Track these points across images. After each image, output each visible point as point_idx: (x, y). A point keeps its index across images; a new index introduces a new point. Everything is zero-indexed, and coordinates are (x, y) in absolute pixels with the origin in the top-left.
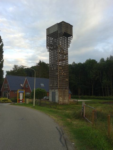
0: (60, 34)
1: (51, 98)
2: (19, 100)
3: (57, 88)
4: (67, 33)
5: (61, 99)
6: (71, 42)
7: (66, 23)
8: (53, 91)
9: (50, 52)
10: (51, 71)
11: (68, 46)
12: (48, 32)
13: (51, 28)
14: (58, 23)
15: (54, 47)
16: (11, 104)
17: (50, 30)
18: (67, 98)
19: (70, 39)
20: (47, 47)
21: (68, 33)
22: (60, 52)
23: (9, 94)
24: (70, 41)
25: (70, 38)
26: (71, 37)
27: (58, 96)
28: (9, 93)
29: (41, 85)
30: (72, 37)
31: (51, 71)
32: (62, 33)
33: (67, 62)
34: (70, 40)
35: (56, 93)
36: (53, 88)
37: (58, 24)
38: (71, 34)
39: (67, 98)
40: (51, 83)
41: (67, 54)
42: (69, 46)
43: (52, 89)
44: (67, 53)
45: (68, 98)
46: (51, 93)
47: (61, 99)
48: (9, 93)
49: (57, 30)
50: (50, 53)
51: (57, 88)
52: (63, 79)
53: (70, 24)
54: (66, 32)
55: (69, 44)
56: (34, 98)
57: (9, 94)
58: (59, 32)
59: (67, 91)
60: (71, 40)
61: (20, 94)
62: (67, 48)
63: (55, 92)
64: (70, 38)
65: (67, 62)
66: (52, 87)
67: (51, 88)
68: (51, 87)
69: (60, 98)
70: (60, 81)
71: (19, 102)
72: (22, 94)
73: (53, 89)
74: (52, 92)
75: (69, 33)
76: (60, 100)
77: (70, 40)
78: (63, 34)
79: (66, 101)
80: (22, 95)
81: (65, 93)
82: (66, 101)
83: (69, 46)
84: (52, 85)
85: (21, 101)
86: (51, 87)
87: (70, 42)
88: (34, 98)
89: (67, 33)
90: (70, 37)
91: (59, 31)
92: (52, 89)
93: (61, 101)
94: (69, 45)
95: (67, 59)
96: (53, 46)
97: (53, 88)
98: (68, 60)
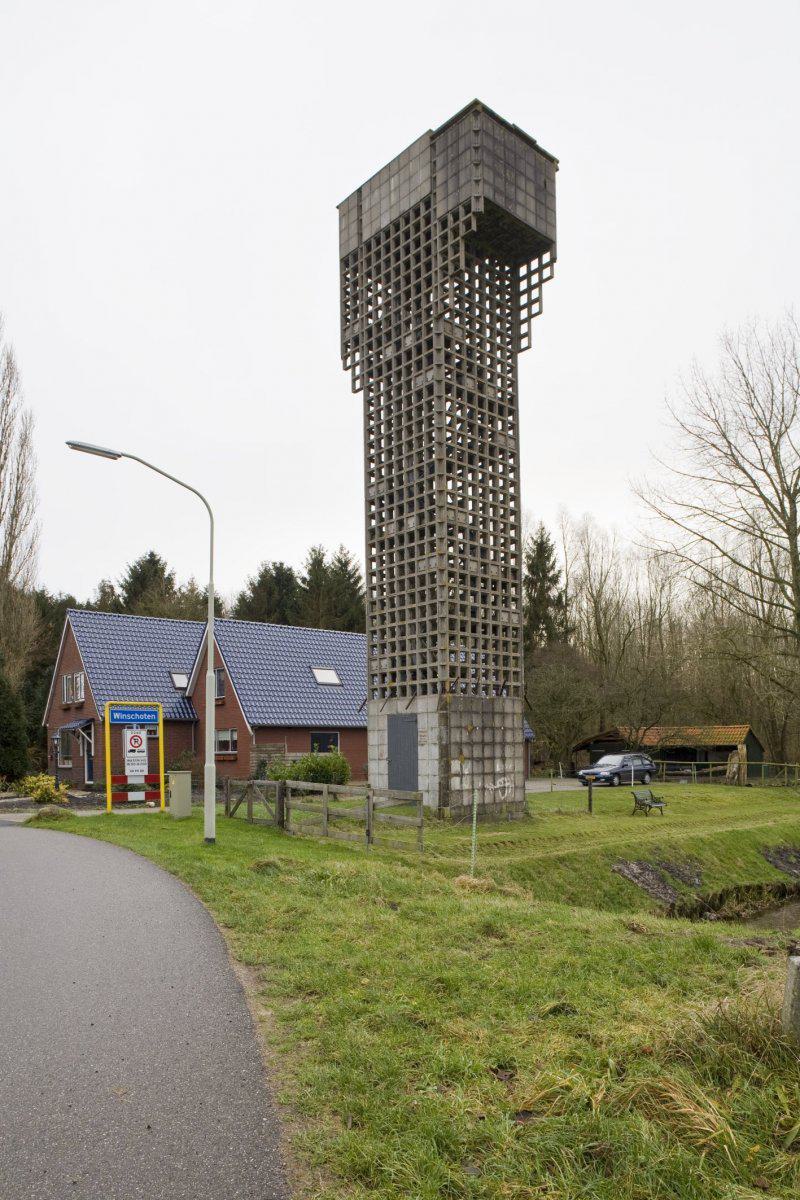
0: (450, 218)
1: (384, 765)
2: (122, 786)
3: (430, 689)
4: (510, 208)
5: (461, 775)
6: (538, 300)
7: (502, 123)
8: (400, 706)
9: (366, 395)
10: (412, 581)
11: (515, 341)
12: (354, 228)
13: (372, 192)
14: (434, 129)
15: (398, 345)
16: (38, 818)
17: (366, 205)
18: (509, 766)
19: (535, 279)
20: (344, 358)
21: (519, 213)
22: (480, 575)
23: (92, 741)
24: (535, 294)
25: (530, 274)
26: (546, 258)
27: (435, 751)
28: (89, 735)
29: (314, 677)
30: (553, 260)
31: (412, 581)
32: (468, 209)
33: (514, 541)
34: (530, 288)
35: (422, 723)
36: (393, 689)
37: (433, 137)
38: (541, 228)
39: (509, 766)
40: (376, 651)
41: (506, 405)
42: (524, 343)
43: (387, 693)
44: (513, 400)
45: (520, 766)
46: (384, 723)
47: (466, 772)
48: (89, 735)
49: (425, 190)
50: (368, 403)
51: (430, 689)
52: (486, 641)
53: (530, 143)
54: (500, 201)
55: (528, 320)
56: (475, 822)
57: (92, 741)
58: (441, 209)
59: (508, 708)
60: (539, 285)
61: (128, 734)
62: (513, 356)
63: (415, 715)
64: (530, 274)
65: (513, 562)
66: (388, 679)
67: (384, 690)
68: (384, 675)
69: (455, 766)
70: (452, 623)
71: (120, 800)
72: (143, 734)
73: (398, 692)
74: (393, 719)
75: (525, 212)
76: (455, 783)
77: (530, 288)
78: (477, 215)
79: (503, 789)
80: (144, 746)
81: (497, 722)
82: (503, 789)
83: (527, 335)
84: (386, 663)
85: (133, 796)
86: (384, 675)
87: (531, 303)
88: (475, 822)
89: (516, 221)
90: (535, 264)
91: (446, 197)
92: (393, 694)
93: (460, 791)
94: (524, 329)
95: (511, 443)
96: (394, 339)
97: (393, 689)
98: (515, 455)
